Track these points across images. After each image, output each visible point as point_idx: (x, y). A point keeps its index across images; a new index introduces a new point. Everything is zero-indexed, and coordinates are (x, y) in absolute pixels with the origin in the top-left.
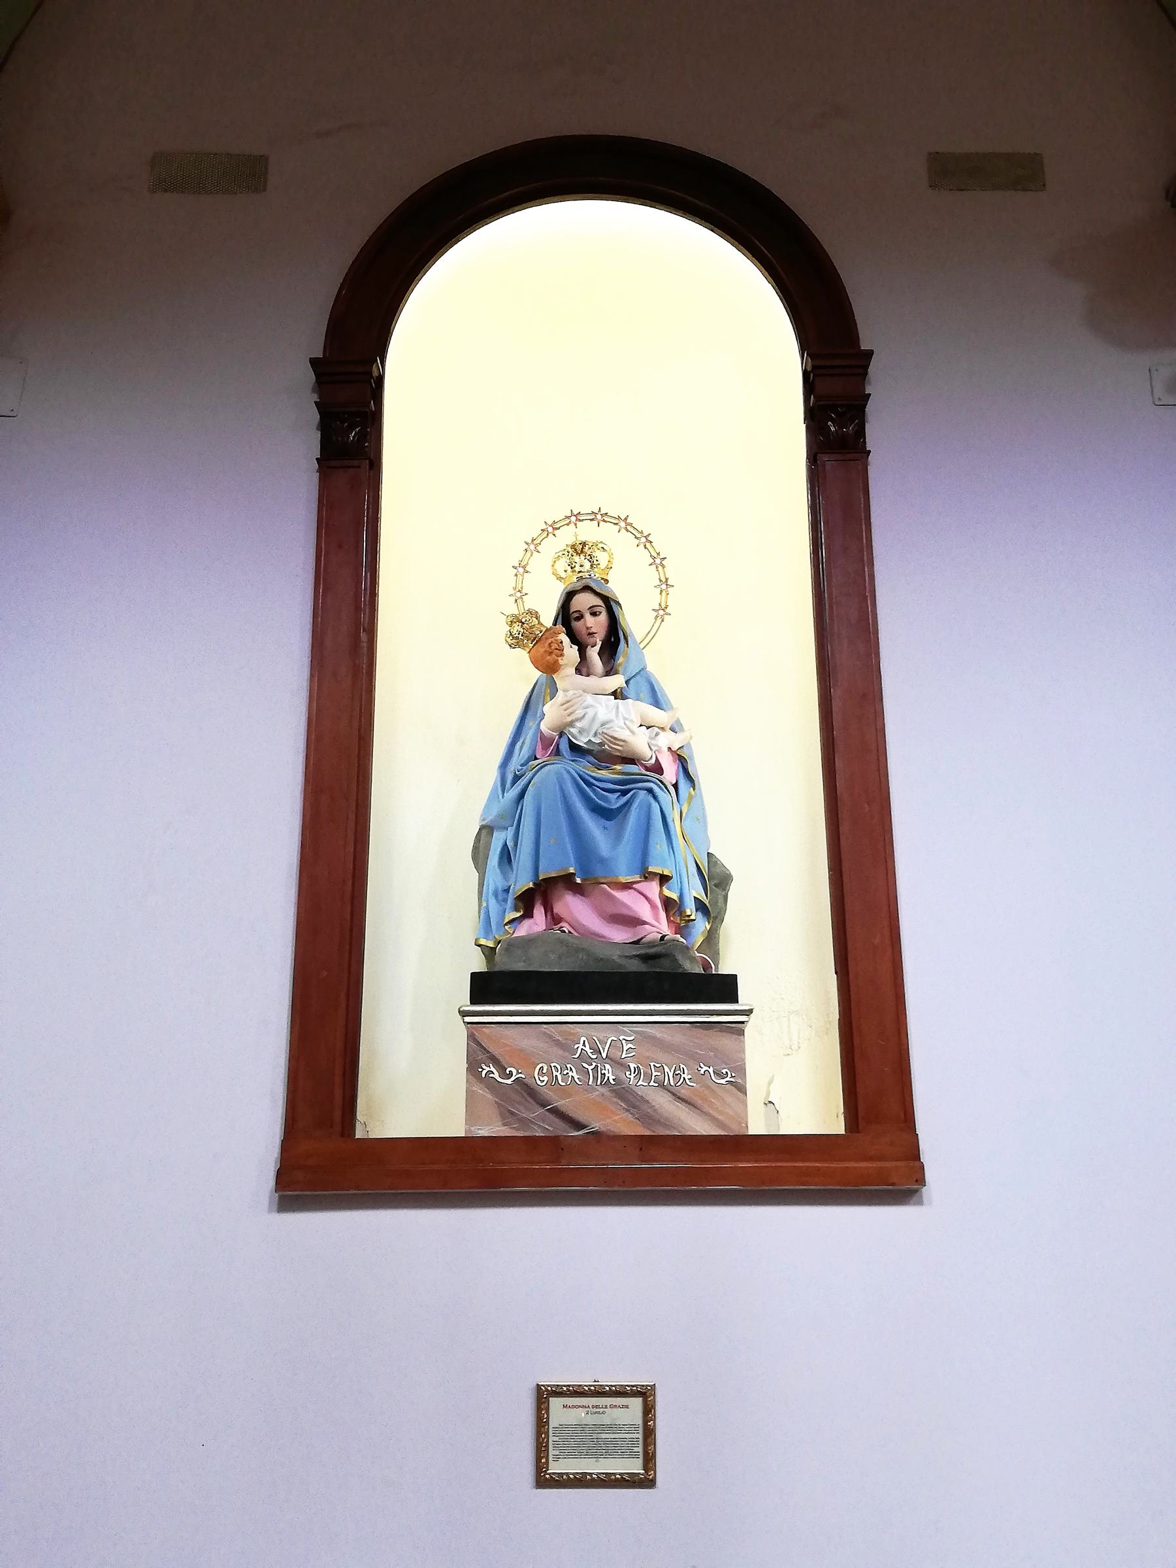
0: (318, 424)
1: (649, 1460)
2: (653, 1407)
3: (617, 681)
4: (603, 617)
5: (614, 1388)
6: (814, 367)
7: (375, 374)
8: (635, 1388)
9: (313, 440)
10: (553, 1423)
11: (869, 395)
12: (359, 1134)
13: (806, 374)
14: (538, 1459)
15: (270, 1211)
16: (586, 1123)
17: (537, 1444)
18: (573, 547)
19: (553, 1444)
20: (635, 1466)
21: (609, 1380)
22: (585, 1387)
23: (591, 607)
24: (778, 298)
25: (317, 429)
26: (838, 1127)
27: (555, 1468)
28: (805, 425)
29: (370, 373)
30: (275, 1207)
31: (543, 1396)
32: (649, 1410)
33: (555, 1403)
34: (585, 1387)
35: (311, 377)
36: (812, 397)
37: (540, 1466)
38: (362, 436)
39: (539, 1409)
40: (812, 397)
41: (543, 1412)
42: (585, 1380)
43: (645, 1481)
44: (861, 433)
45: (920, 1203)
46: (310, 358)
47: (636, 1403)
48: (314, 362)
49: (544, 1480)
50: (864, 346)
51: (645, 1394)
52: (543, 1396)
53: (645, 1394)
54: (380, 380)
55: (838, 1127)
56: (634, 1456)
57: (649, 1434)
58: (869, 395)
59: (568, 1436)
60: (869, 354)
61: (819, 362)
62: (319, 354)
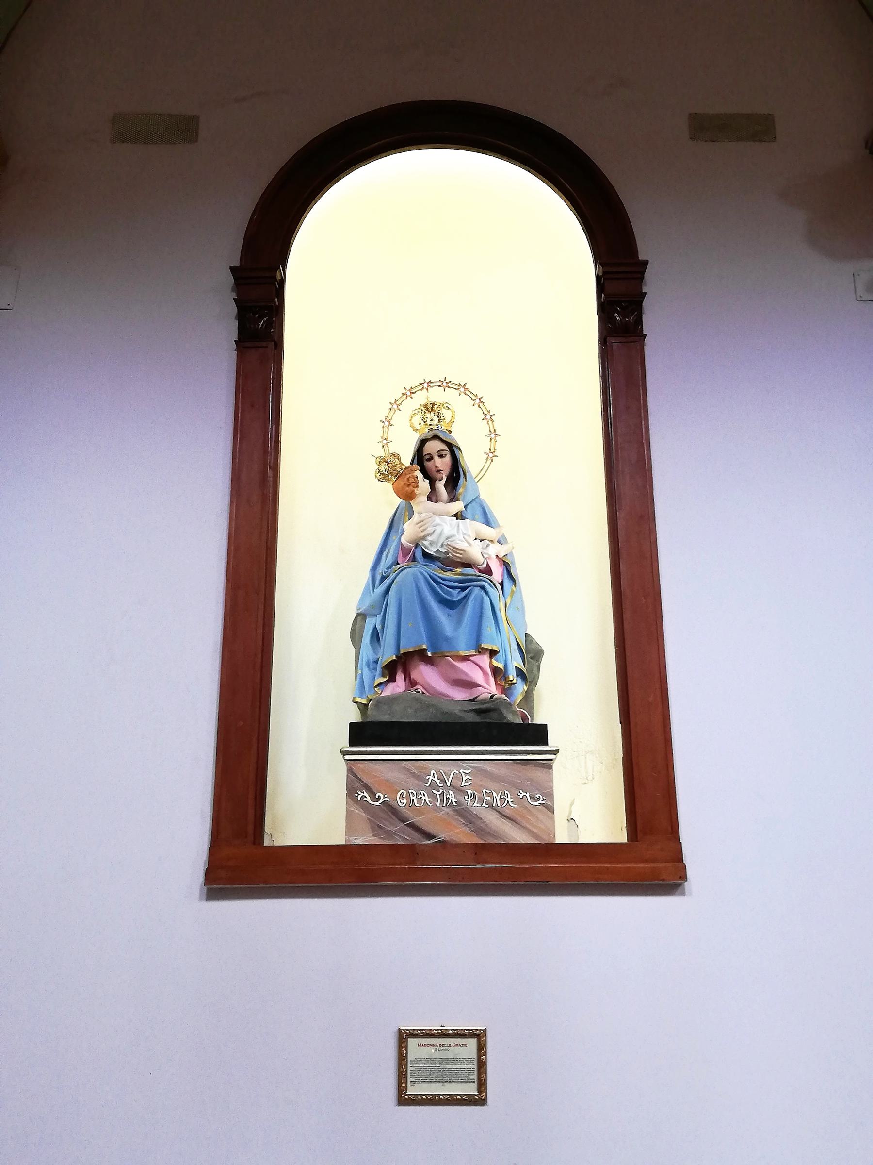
0: (236, 315)
1: (482, 1084)
2: (485, 1045)
3: (458, 506)
4: (448, 459)
5: (456, 1031)
6: (604, 273)
7: (279, 278)
8: (471, 1031)
9: (233, 327)
10: (411, 1057)
11: (645, 293)
12: (266, 843)
13: (598, 278)
14: (399, 1084)
15: (200, 900)
16: (435, 834)
17: (399, 1073)
18: (425, 406)
19: (411, 1073)
20: (471, 1090)
21: (452, 1025)
22: (434, 1031)
23: (439, 451)
24: (578, 221)
25: (236, 319)
26: (622, 837)
27: (412, 1091)
28: (597, 316)
29: (275, 277)
30: (204, 897)
31: (403, 1037)
32: (481, 1048)
33: (412, 1042)
34: (434, 1031)
35: (231, 280)
36: (603, 295)
37: (401, 1090)
38: (269, 324)
39: (400, 1047)
40: (603, 295)
41: (403, 1049)
42: (434, 1025)
43: (479, 1101)
44: (639, 321)
45: (683, 893)
46: (230, 266)
47: (472, 1043)
48: (233, 269)
49: (404, 1100)
50: (641, 257)
51: (479, 1036)
52: (403, 1037)
53: (479, 1036)
54: (282, 282)
55: (622, 837)
56: (471, 1081)
57: (482, 1065)
58: (645, 293)
59: (422, 1067)
60: (645, 263)
61: (608, 269)
62: (237, 263)
